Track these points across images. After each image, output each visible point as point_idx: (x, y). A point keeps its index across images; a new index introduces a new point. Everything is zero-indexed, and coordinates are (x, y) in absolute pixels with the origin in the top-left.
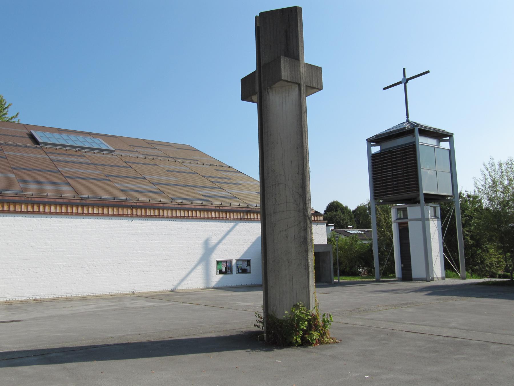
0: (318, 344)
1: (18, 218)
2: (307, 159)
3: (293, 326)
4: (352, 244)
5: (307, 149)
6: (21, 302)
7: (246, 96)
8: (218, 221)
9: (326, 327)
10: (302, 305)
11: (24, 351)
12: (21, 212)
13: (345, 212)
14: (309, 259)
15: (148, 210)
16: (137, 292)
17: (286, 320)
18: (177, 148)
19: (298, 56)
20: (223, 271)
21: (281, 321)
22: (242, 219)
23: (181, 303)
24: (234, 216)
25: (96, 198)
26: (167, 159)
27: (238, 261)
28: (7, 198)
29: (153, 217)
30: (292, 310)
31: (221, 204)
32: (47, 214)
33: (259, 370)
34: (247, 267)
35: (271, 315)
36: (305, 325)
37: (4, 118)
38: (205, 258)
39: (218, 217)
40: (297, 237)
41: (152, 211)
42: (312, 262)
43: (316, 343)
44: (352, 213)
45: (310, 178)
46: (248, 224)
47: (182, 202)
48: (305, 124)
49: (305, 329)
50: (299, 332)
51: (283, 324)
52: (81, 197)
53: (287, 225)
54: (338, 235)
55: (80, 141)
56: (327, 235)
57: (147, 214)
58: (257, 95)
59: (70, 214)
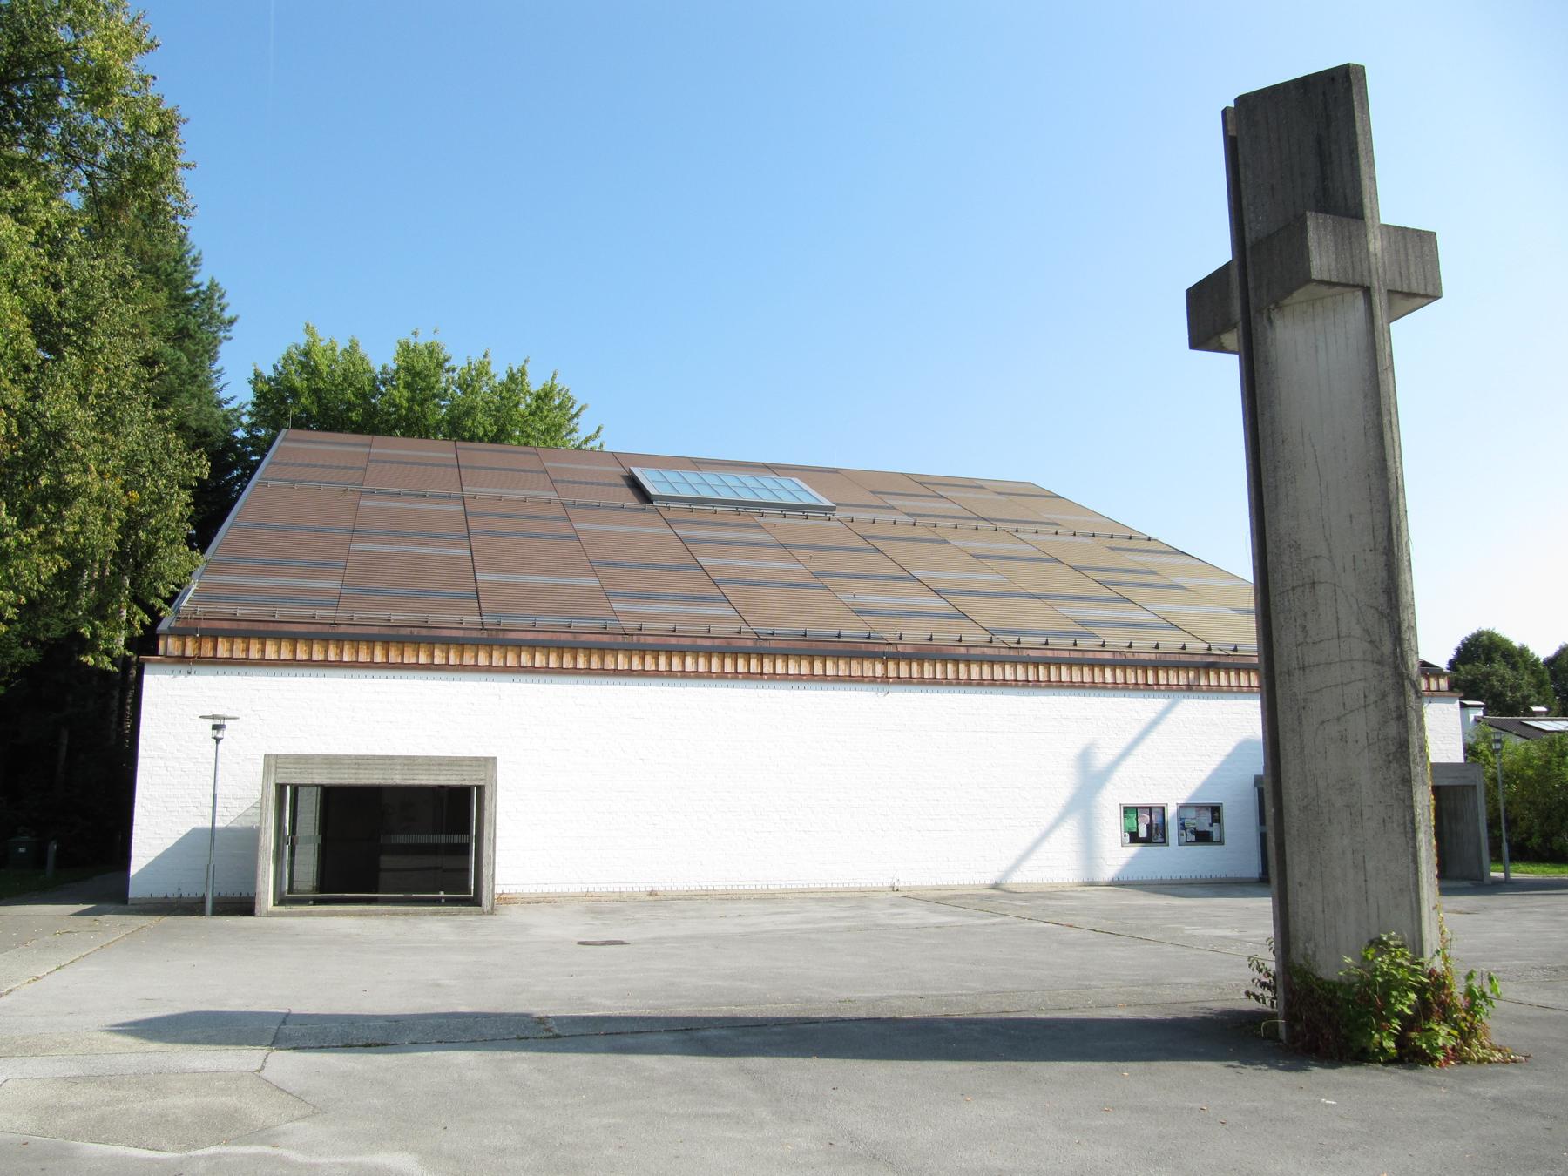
0: (1453, 1063)
1: (609, 687)
2: (1401, 507)
3: (1370, 1001)
4: (1549, 762)
5: (1399, 478)
6: (621, 898)
7: (1203, 336)
8: (1122, 693)
9: (1477, 1013)
10: (1396, 942)
11: (650, 1018)
12: (616, 673)
13: (1521, 664)
14: (1415, 804)
15: (926, 665)
16: (902, 884)
17: (1347, 983)
18: (999, 491)
19: (1360, 205)
20: (1140, 836)
21: (1331, 987)
22: (1194, 688)
23: (1023, 921)
24: (1168, 679)
25: (856, 637)
26: (974, 523)
27: (1183, 807)
28: (584, 638)
29: (941, 684)
30: (1364, 953)
31: (1130, 646)
32: (676, 677)
33: (1271, 1120)
34: (1211, 825)
35: (1301, 965)
36: (1407, 1002)
37: (570, 440)
38: (1082, 804)
39: (1123, 681)
40: (1376, 740)
41: (938, 666)
42: (1426, 814)
43: (1447, 1058)
44: (1542, 667)
45: (1410, 564)
46: (1212, 702)
47: (1019, 642)
48: (1389, 404)
49: (1410, 1015)
50: (1388, 1021)
51: (1339, 994)
52: (755, 633)
53: (1344, 704)
54: (1501, 733)
55: (746, 486)
56: (1465, 734)
57: (926, 676)
58: (1238, 330)
59: (729, 676)
